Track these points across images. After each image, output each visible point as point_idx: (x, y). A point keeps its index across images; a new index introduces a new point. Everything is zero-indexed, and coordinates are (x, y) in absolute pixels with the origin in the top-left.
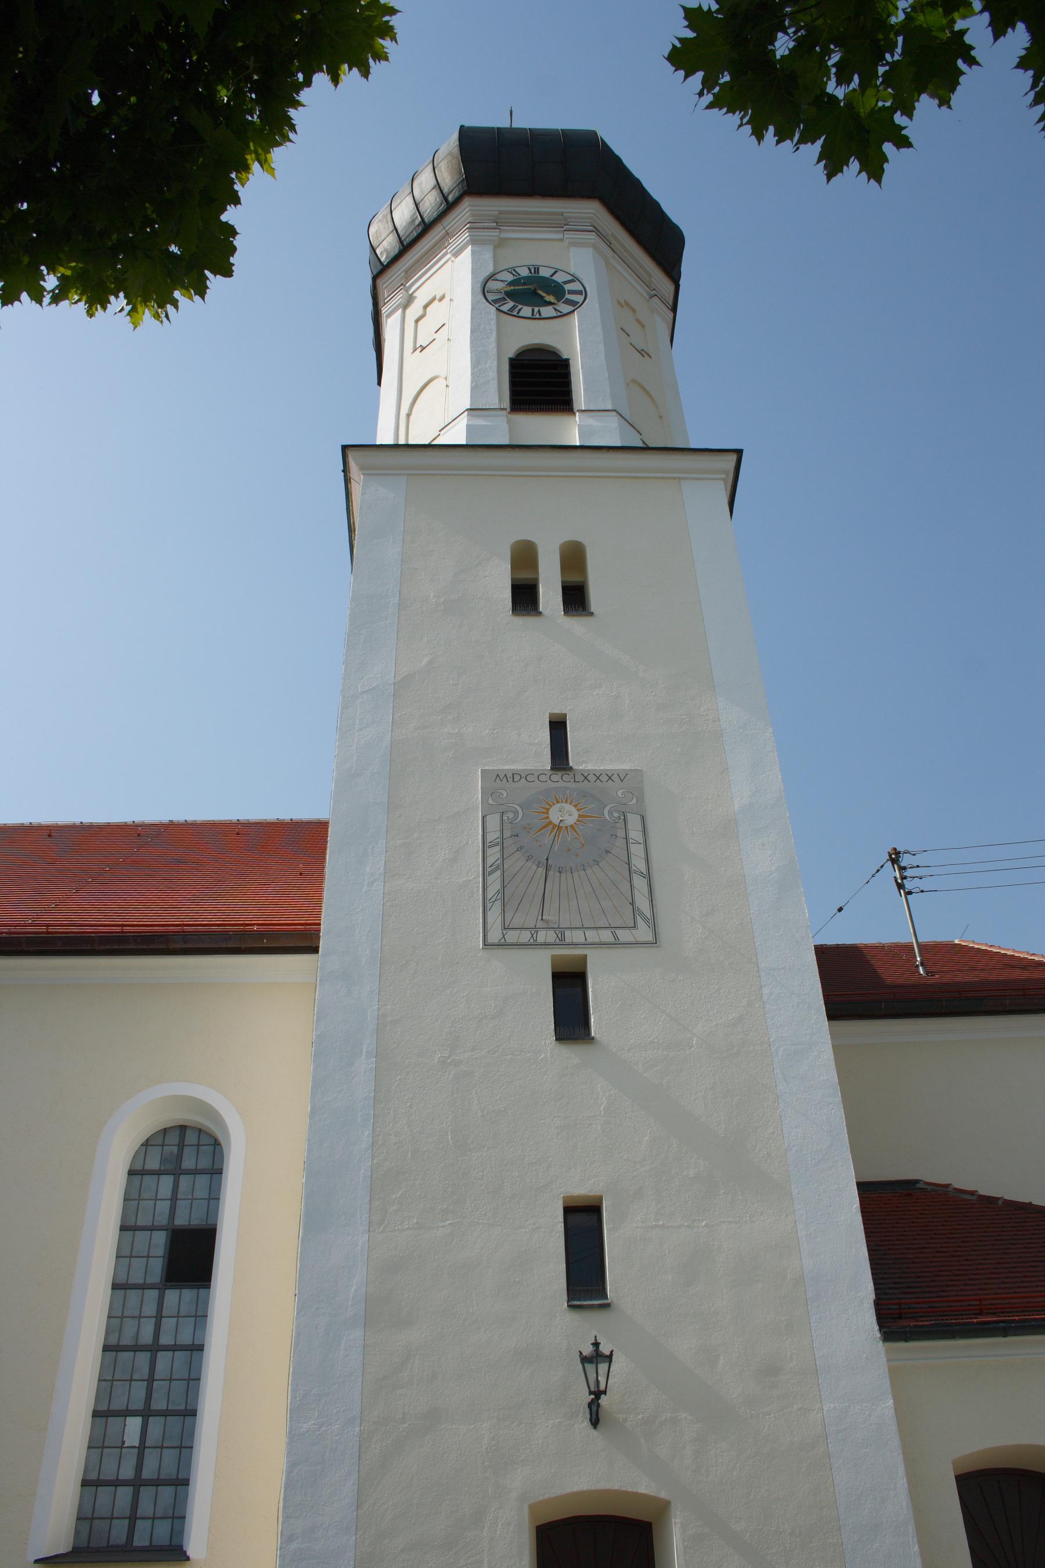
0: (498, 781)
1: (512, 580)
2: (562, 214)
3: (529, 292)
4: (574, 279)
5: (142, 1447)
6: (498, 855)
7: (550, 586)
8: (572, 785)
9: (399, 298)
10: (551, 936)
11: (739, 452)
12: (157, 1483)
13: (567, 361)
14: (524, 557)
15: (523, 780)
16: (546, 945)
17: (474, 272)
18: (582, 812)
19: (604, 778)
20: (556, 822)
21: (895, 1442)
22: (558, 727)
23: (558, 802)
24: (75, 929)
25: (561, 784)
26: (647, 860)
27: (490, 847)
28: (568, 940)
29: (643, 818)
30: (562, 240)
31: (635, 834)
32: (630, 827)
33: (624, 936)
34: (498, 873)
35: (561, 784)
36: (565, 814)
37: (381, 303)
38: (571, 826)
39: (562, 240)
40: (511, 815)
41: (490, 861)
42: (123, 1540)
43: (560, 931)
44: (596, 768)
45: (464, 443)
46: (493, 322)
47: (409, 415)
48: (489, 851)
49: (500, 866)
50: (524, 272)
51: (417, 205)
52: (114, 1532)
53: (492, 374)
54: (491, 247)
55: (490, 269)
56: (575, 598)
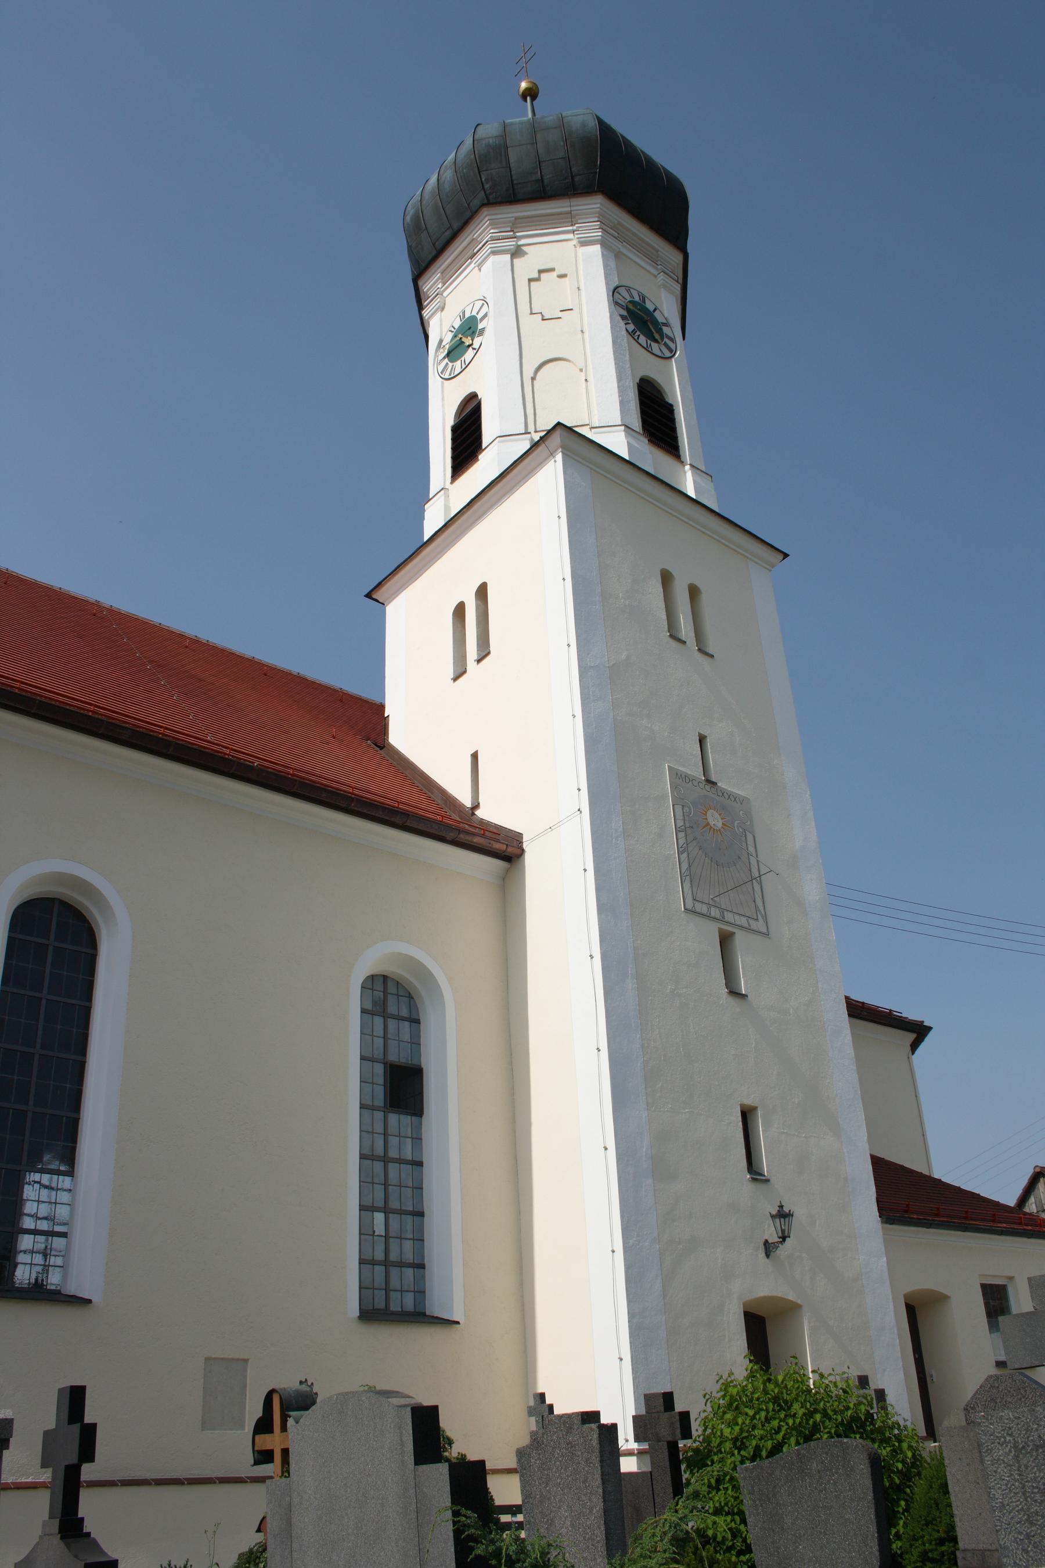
2: (657, 251)
5: (387, 1237)
12: (402, 1265)
13: (671, 406)
17: (607, 284)
21: (888, 1283)
24: (334, 785)
25: (710, 794)
33: (754, 925)
42: (383, 1305)
43: (723, 910)
52: (376, 1300)
55: (616, 284)
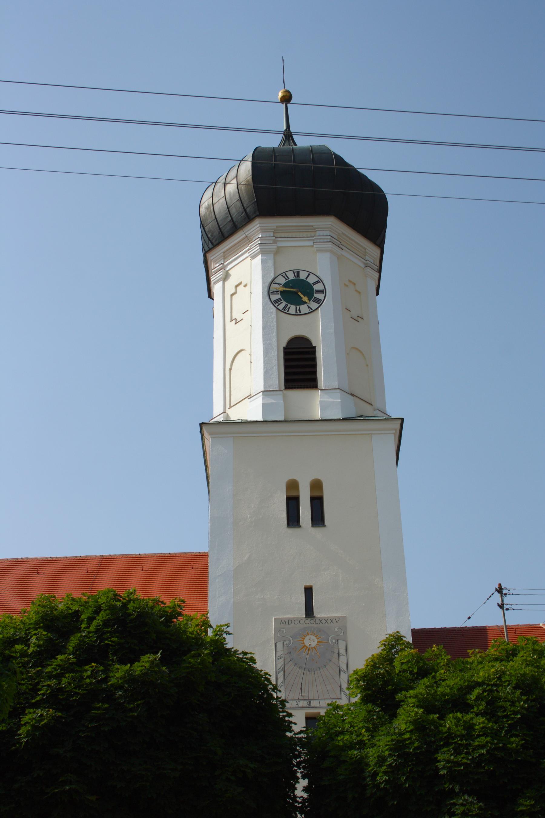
0: (282, 623)
1: (287, 496)
3: (292, 293)
4: (320, 281)
6: (282, 663)
7: (305, 507)
8: (315, 625)
9: (220, 274)
10: (305, 704)
11: (402, 420)
13: (315, 347)
14: (293, 485)
15: (293, 623)
16: (303, 708)
18: (319, 640)
19: (329, 621)
20: (308, 645)
22: (308, 591)
23: (308, 635)
25: (310, 625)
26: (347, 664)
27: (279, 659)
28: (312, 705)
29: (346, 642)
30: (312, 246)
31: (342, 651)
32: (340, 647)
34: (282, 672)
35: (310, 625)
36: (311, 641)
37: (210, 275)
38: (314, 647)
39: (312, 246)
40: (287, 642)
41: (279, 666)
43: (309, 701)
44: (326, 616)
45: (260, 419)
46: (274, 315)
47: (230, 369)
48: (279, 661)
49: (283, 669)
50: (291, 276)
51: (228, 208)
53: (275, 362)
54: (272, 255)
55: (272, 276)
56: (318, 518)
